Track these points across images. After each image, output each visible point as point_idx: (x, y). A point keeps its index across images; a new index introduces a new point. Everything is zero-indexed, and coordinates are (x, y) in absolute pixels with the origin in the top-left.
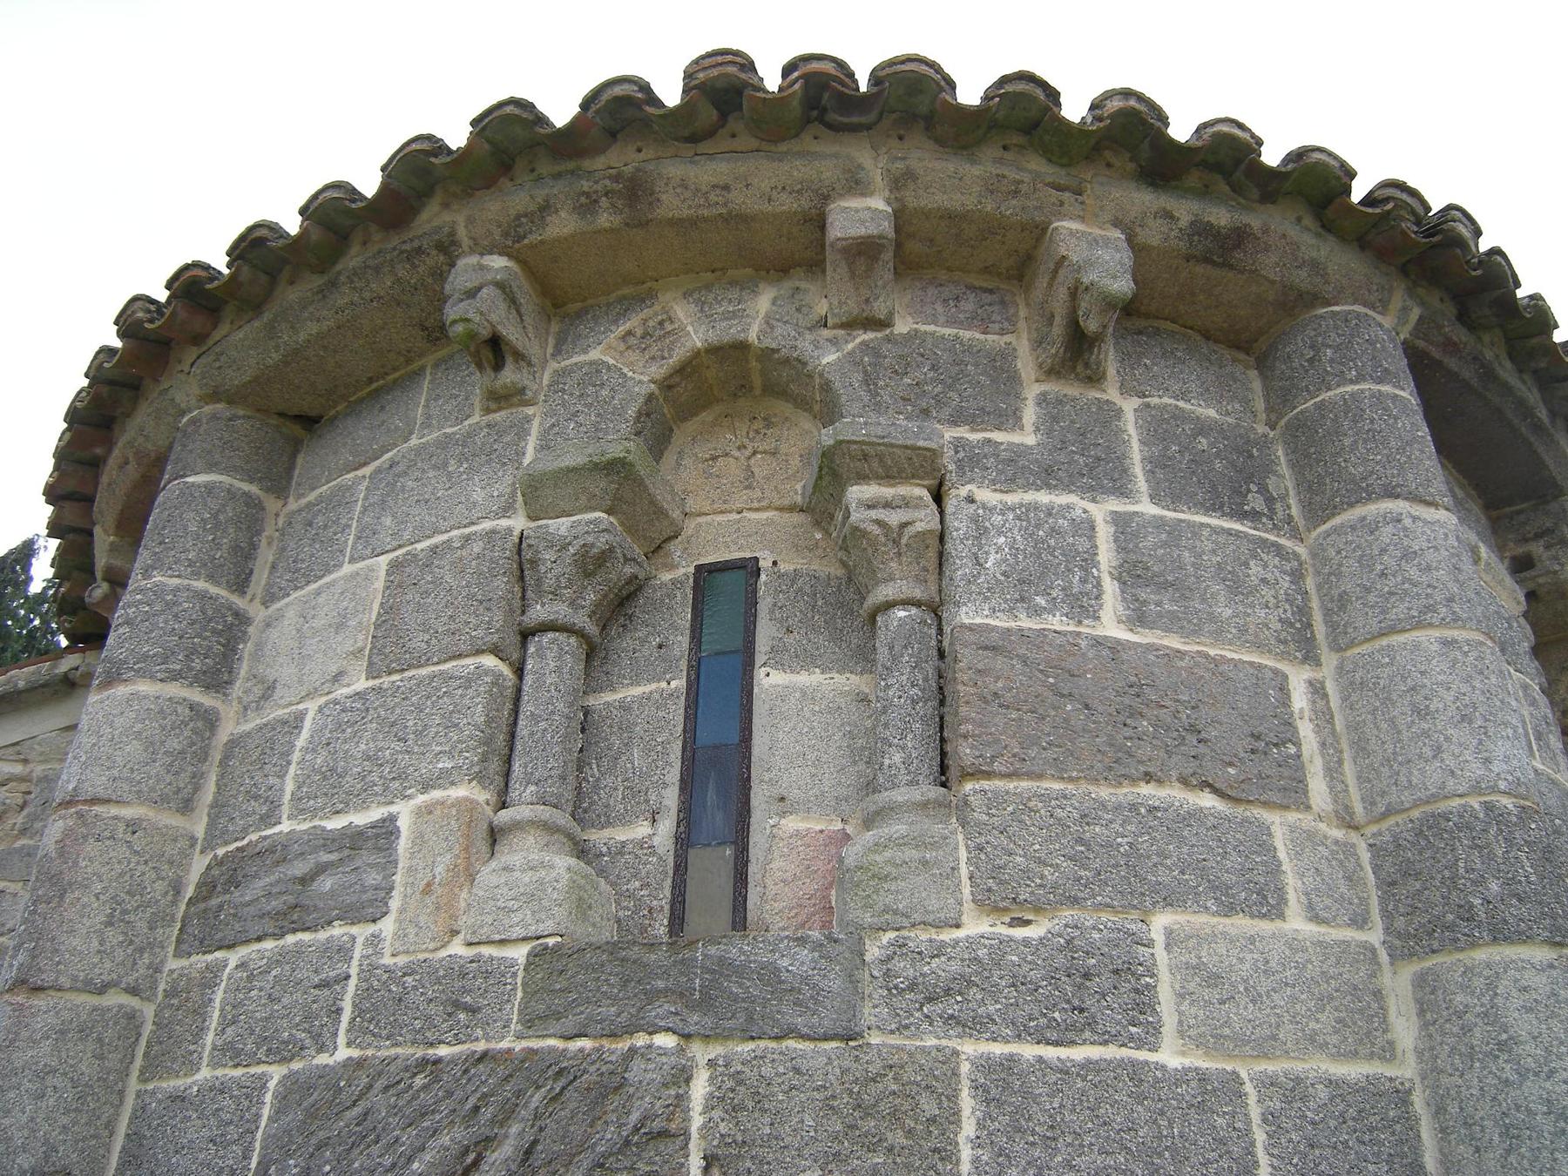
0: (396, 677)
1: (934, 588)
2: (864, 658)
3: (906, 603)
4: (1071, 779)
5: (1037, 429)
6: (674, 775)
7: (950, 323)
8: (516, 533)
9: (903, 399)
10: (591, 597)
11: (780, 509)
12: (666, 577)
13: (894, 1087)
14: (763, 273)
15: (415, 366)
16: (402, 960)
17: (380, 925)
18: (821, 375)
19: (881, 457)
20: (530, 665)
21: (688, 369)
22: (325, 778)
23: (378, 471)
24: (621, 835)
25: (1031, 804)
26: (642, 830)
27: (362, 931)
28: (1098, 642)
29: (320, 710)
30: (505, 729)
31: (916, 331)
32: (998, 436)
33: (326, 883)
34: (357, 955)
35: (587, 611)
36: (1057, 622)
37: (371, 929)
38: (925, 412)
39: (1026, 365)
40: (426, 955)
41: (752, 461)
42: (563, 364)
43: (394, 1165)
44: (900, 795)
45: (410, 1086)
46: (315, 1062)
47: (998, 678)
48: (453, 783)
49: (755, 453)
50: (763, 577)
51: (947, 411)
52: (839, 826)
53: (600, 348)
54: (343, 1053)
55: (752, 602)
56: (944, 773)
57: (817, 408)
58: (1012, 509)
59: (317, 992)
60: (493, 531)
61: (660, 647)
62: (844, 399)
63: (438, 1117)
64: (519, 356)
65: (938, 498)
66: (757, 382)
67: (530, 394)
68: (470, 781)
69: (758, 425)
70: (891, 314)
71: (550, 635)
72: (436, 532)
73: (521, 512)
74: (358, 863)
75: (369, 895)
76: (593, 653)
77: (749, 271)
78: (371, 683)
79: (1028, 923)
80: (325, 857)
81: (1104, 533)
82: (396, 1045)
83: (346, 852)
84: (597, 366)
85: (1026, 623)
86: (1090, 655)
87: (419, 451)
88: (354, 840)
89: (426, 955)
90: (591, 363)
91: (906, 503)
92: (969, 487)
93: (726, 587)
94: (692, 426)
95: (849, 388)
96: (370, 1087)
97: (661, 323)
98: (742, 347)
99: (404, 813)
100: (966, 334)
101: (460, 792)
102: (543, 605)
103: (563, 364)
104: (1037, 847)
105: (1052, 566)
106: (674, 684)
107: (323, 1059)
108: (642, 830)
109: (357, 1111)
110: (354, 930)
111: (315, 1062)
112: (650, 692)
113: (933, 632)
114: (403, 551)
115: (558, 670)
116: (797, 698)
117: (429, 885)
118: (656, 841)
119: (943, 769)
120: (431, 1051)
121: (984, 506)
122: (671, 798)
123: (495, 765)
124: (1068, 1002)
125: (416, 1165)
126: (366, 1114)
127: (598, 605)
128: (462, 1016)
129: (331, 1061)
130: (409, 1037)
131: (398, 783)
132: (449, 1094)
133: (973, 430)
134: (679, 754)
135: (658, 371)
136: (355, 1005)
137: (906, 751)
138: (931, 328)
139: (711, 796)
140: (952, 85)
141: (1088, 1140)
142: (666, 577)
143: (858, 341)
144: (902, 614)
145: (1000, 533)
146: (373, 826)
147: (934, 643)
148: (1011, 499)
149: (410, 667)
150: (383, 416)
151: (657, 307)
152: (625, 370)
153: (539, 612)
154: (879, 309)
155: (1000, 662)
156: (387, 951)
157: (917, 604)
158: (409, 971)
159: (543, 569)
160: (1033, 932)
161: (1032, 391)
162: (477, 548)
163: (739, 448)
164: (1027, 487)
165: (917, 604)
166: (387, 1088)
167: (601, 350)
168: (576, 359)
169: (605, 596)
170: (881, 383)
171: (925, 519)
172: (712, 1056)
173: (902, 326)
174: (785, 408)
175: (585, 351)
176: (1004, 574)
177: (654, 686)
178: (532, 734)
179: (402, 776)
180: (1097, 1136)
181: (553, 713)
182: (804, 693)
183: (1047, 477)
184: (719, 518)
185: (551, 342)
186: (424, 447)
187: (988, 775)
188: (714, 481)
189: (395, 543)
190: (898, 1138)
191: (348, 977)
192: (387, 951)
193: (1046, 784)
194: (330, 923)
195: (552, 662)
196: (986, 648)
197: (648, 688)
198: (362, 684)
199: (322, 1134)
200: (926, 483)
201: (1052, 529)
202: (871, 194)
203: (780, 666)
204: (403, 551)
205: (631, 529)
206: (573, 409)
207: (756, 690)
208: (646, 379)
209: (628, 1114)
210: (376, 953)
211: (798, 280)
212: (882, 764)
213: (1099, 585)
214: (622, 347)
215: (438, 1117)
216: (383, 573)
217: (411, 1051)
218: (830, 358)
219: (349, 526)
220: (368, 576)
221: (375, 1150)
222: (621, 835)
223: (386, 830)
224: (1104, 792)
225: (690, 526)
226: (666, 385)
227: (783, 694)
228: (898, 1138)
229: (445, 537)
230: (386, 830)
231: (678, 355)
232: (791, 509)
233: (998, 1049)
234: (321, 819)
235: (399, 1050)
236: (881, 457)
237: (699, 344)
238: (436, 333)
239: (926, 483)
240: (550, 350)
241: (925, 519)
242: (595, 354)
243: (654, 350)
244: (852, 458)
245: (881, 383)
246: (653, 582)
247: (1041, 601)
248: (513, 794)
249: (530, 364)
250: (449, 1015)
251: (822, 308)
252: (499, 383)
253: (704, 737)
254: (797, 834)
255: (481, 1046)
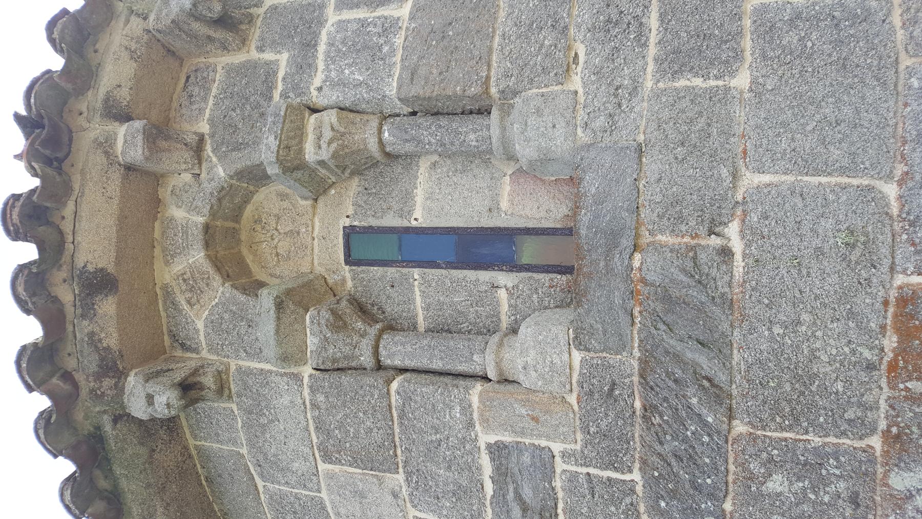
0: (399, 452)
1: (372, 117)
2: (408, 160)
3: (380, 131)
4: (494, 32)
5: (279, 52)
6: (471, 274)
7: (205, 99)
8: (314, 372)
9: (252, 127)
10: (359, 325)
11: (314, 215)
12: (350, 284)
13: (671, 124)
14: (159, 215)
15: (194, 452)
16: (579, 436)
17: (556, 453)
18: (231, 177)
19: (289, 138)
20: (397, 363)
21: (217, 264)
22: (460, 499)
23: (262, 476)
24: (505, 308)
25: (507, 53)
26: (502, 294)
27: (560, 465)
28: (412, 18)
29: (415, 506)
30: (437, 378)
31: (208, 120)
32: (281, 74)
33: (527, 493)
34: (574, 468)
35: (368, 328)
36: (399, 40)
37: (558, 459)
38: (262, 115)
39: (238, 58)
40: (577, 418)
41: (282, 231)
42: (204, 346)
43: (709, 435)
44: (495, 132)
45: (660, 425)
46: (641, 495)
47: (431, 73)
48: (470, 406)
49: (276, 229)
50: (356, 223)
51: (262, 102)
52: (508, 178)
53: (197, 321)
54: (636, 476)
55: (370, 230)
56: (485, 111)
57: (251, 188)
58: (327, 66)
59: (597, 496)
60: (311, 387)
61: (393, 286)
62: (248, 163)
63: (680, 407)
64: (195, 372)
65: (314, 111)
66: (230, 224)
67: (222, 368)
68: (469, 394)
69: (258, 228)
70: (195, 133)
71: (381, 349)
72: (307, 429)
73: (301, 369)
74: (516, 470)
75: (537, 460)
76: (391, 328)
77: (157, 224)
78: (401, 470)
79: (576, 54)
80: (511, 495)
81: (347, 15)
82: (633, 436)
83: (509, 479)
84: (209, 323)
85: (398, 58)
86: (420, 22)
87: (251, 445)
88: (501, 475)
89: (577, 418)
90: (206, 326)
91: (319, 127)
92: (312, 90)
93: (359, 245)
94: (254, 268)
95: (242, 161)
96: (660, 455)
97: (185, 280)
98: (207, 228)
99: (485, 438)
100: (214, 91)
101: (475, 400)
102: (361, 355)
103: (204, 346)
104: (533, 49)
105: (364, 46)
106: (416, 277)
107: (639, 489)
108: (502, 294)
109: (674, 462)
110: (558, 470)
111: (641, 495)
112: (420, 291)
113: (398, 119)
114: (316, 452)
115: (403, 344)
116: (433, 199)
117: (533, 419)
118: (510, 285)
119: (479, 112)
120: (638, 413)
121: (325, 81)
122: (484, 276)
123: (461, 382)
124: (625, 31)
125: (710, 420)
126: (676, 456)
127: (364, 322)
128: (617, 392)
129: (641, 483)
130: (628, 429)
131: (468, 442)
132: (665, 399)
133: (276, 88)
134: (459, 271)
135: (217, 281)
136: (606, 469)
137: (470, 133)
138: (208, 112)
139: (485, 251)
140: (49, 72)
141: (705, 17)
142: (350, 284)
143: (211, 154)
144: (386, 134)
145: (342, 72)
146: (492, 460)
147: (405, 118)
148: (321, 65)
149: (393, 441)
150: (226, 476)
151: (174, 284)
152: (214, 303)
153: (366, 359)
154: (191, 139)
155: (422, 71)
156: (573, 446)
157: (381, 125)
158: (586, 430)
159: (339, 354)
160: (581, 50)
161: (254, 55)
162: (321, 398)
163: (273, 239)
164: (315, 57)
165: (381, 125)
166: (661, 443)
167: (199, 323)
168: (202, 338)
169: (359, 317)
170: (240, 140)
171: (331, 117)
172: (647, 233)
173: (204, 128)
174: (249, 210)
175: (197, 331)
176: (367, 70)
177: (416, 289)
178: (441, 358)
179: (463, 441)
180: (704, 13)
181: (430, 346)
182: (427, 199)
183: (310, 45)
184: (316, 251)
185: (189, 355)
186: (249, 440)
187: (488, 78)
188: (292, 254)
189: (311, 458)
190: (702, 122)
191: (588, 474)
192: (573, 446)
193: (495, 45)
194: (553, 489)
195: (396, 351)
196: (412, 79)
197: (417, 293)
198: (401, 477)
199: (687, 486)
200: (307, 115)
201: (343, 43)
202: (116, 134)
203: (410, 213)
204: (316, 452)
205: (319, 302)
206: (227, 118)
207: (424, 226)
208: (221, 289)
209: (682, 282)
210: (574, 455)
211: (165, 193)
212: (475, 146)
213: (379, 18)
214: (197, 307)
215: (680, 407)
216: (330, 467)
217: (637, 426)
218: (221, 172)
219: (296, 494)
220: (331, 476)
221: (699, 449)
222: (505, 308)
223: (497, 451)
224: (502, 14)
225: (319, 270)
226: (227, 277)
227: (428, 210)
228: (702, 122)
229: (311, 422)
230: (497, 451)
231: (208, 268)
232: (314, 207)
233: (651, 68)
234: (485, 499)
235: (637, 435)
236: (289, 138)
237: (202, 254)
238: (171, 424)
239: (307, 115)
240: (194, 355)
241: (331, 117)
242: (200, 325)
243: (202, 285)
244: (287, 155)
245: (240, 140)
246: (352, 293)
247: (386, 49)
248: (478, 370)
249: (202, 367)
250: (616, 401)
251: (187, 177)
252: (213, 387)
253: (452, 258)
254: (511, 202)
255: (636, 379)
